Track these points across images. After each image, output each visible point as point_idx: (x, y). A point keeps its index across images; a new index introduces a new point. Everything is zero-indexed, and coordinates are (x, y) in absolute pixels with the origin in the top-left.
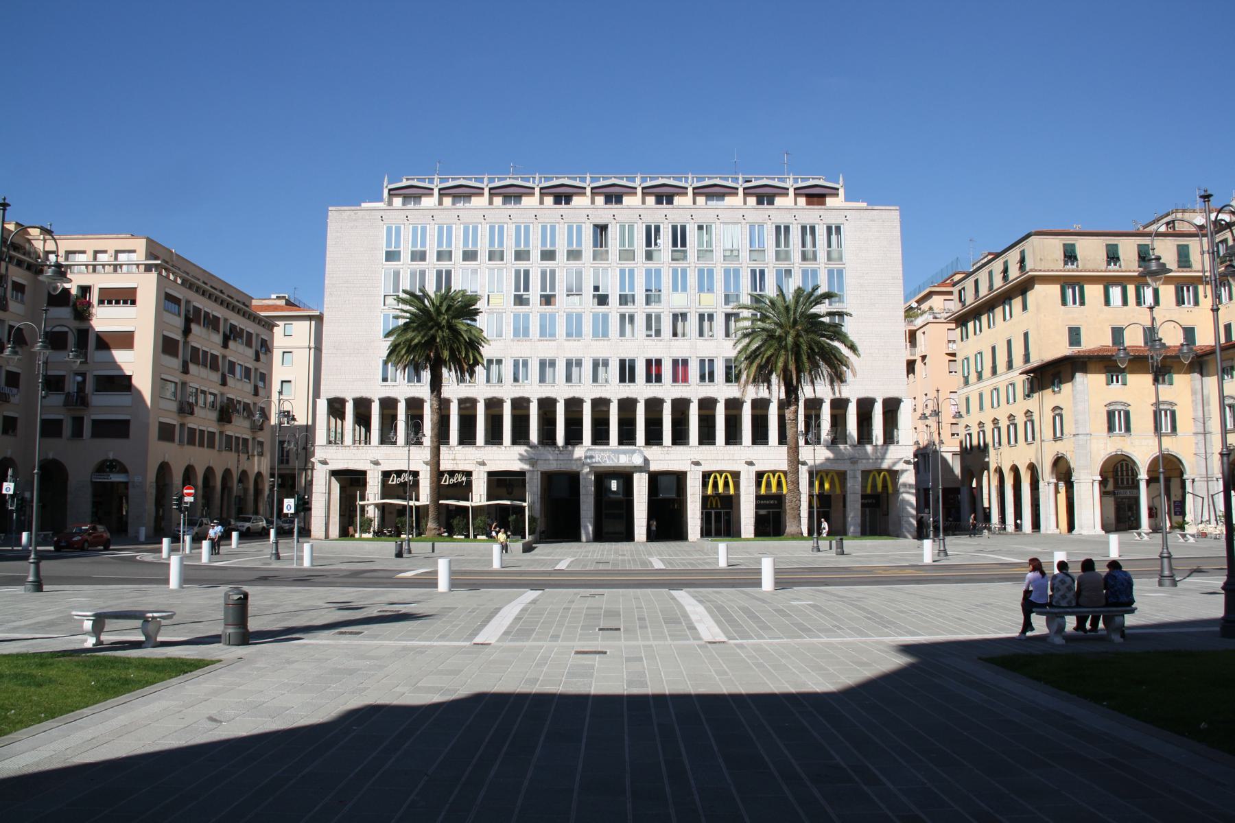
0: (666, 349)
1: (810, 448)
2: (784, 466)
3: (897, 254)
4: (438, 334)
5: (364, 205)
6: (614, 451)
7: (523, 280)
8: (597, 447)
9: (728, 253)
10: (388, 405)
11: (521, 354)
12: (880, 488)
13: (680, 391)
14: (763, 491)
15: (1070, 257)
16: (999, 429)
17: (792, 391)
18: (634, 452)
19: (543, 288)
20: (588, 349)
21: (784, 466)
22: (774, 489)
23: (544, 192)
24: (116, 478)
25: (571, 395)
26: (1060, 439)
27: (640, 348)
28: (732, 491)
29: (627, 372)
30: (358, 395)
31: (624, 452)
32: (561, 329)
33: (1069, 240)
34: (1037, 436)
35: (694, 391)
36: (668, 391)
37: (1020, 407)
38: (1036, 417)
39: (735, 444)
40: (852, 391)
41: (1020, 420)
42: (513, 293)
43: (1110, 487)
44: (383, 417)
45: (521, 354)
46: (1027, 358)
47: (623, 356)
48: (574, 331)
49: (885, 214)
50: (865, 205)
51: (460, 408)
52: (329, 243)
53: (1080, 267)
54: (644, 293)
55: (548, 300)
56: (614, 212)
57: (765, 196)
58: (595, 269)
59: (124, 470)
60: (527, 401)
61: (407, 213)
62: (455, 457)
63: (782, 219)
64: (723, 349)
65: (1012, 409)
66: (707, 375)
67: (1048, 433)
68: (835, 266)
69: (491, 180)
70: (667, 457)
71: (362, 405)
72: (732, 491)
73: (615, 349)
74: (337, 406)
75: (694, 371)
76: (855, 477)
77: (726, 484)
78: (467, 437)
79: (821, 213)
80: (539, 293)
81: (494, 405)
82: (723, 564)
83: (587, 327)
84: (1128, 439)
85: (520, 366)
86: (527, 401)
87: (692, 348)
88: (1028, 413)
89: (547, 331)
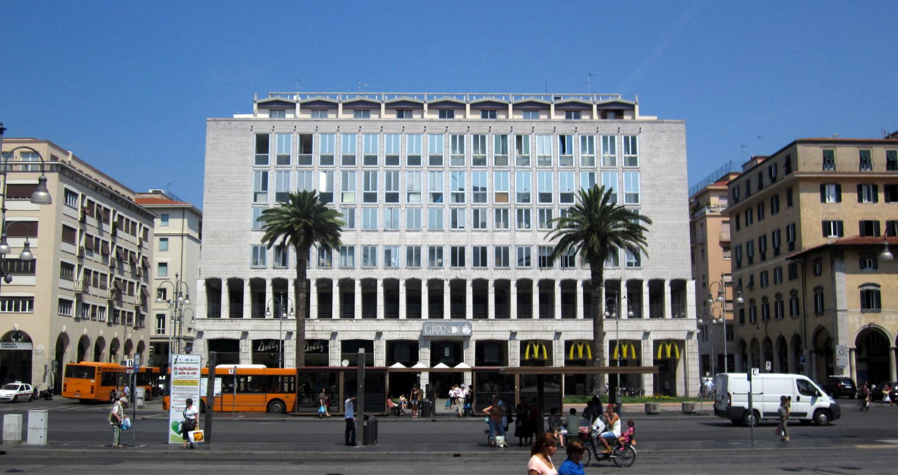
0: (491, 238)
1: (614, 322)
2: (590, 336)
3: (683, 159)
4: (306, 223)
5: (236, 116)
6: (446, 324)
7: (369, 180)
8: (433, 321)
9: (542, 159)
10: (258, 285)
11: (378, 239)
12: (669, 355)
13: (501, 274)
14: (571, 357)
15: (829, 162)
16: (782, 303)
17: (597, 273)
18: (463, 324)
19: (388, 187)
20: (425, 240)
21: (590, 336)
22: (581, 355)
23: (474, 107)
24: (21, 346)
25: (411, 276)
26: (822, 314)
27: (469, 239)
28: (546, 357)
29: (458, 256)
30: (231, 276)
31: (456, 325)
32: (403, 221)
33: (829, 148)
34: (801, 311)
35: (513, 274)
36: (491, 274)
37: (786, 287)
38: (800, 295)
39: (658, 317)
40: (644, 274)
41: (786, 298)
42: (363, 191)
43: (864, 355)
44: (276, 295)
45: (378, 239)
46: (792, 247)
47: (454, 244)
48: (414, 225)
49: (674, 127)
50: (655, 118)
51: (319, 288)
52: (208, 147)
53: (838, 169)
54: (472, 192)
55: (392, 198)
56: (447, 124)
57: (447, 109)
58: (344, 172)
59: (28, 340)
60: (374, 281)
61: (274, 124)
62: (317, 329)
63: (502, 129)
64: (539, 238)
65: (779, 288)
66: (524, 260)
67: (811, 308)
68: (262, 168)
69: (430, 97)
70: (403, 328)
71: (236, 286)
72: (546, 357)
73: (447, 239)
74: (214, 285)
75: (513, 257)
76: (648, 346)
77: (541, 351)
78: (325, 312)
79: (620, 125)
80: (385, 191)
81: (347, 286)
82: (202, 431)
83: (424, 221)
84: (879, 315)
85: (369, 253)
86: (374, 281)
87: (515, 237)
88: (793, 292)
89: (393, 226)
